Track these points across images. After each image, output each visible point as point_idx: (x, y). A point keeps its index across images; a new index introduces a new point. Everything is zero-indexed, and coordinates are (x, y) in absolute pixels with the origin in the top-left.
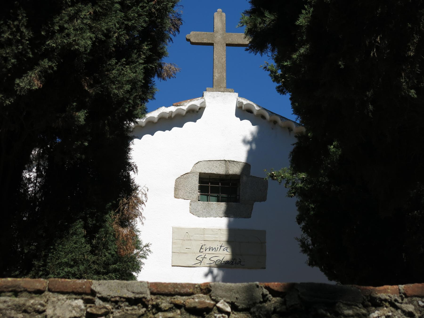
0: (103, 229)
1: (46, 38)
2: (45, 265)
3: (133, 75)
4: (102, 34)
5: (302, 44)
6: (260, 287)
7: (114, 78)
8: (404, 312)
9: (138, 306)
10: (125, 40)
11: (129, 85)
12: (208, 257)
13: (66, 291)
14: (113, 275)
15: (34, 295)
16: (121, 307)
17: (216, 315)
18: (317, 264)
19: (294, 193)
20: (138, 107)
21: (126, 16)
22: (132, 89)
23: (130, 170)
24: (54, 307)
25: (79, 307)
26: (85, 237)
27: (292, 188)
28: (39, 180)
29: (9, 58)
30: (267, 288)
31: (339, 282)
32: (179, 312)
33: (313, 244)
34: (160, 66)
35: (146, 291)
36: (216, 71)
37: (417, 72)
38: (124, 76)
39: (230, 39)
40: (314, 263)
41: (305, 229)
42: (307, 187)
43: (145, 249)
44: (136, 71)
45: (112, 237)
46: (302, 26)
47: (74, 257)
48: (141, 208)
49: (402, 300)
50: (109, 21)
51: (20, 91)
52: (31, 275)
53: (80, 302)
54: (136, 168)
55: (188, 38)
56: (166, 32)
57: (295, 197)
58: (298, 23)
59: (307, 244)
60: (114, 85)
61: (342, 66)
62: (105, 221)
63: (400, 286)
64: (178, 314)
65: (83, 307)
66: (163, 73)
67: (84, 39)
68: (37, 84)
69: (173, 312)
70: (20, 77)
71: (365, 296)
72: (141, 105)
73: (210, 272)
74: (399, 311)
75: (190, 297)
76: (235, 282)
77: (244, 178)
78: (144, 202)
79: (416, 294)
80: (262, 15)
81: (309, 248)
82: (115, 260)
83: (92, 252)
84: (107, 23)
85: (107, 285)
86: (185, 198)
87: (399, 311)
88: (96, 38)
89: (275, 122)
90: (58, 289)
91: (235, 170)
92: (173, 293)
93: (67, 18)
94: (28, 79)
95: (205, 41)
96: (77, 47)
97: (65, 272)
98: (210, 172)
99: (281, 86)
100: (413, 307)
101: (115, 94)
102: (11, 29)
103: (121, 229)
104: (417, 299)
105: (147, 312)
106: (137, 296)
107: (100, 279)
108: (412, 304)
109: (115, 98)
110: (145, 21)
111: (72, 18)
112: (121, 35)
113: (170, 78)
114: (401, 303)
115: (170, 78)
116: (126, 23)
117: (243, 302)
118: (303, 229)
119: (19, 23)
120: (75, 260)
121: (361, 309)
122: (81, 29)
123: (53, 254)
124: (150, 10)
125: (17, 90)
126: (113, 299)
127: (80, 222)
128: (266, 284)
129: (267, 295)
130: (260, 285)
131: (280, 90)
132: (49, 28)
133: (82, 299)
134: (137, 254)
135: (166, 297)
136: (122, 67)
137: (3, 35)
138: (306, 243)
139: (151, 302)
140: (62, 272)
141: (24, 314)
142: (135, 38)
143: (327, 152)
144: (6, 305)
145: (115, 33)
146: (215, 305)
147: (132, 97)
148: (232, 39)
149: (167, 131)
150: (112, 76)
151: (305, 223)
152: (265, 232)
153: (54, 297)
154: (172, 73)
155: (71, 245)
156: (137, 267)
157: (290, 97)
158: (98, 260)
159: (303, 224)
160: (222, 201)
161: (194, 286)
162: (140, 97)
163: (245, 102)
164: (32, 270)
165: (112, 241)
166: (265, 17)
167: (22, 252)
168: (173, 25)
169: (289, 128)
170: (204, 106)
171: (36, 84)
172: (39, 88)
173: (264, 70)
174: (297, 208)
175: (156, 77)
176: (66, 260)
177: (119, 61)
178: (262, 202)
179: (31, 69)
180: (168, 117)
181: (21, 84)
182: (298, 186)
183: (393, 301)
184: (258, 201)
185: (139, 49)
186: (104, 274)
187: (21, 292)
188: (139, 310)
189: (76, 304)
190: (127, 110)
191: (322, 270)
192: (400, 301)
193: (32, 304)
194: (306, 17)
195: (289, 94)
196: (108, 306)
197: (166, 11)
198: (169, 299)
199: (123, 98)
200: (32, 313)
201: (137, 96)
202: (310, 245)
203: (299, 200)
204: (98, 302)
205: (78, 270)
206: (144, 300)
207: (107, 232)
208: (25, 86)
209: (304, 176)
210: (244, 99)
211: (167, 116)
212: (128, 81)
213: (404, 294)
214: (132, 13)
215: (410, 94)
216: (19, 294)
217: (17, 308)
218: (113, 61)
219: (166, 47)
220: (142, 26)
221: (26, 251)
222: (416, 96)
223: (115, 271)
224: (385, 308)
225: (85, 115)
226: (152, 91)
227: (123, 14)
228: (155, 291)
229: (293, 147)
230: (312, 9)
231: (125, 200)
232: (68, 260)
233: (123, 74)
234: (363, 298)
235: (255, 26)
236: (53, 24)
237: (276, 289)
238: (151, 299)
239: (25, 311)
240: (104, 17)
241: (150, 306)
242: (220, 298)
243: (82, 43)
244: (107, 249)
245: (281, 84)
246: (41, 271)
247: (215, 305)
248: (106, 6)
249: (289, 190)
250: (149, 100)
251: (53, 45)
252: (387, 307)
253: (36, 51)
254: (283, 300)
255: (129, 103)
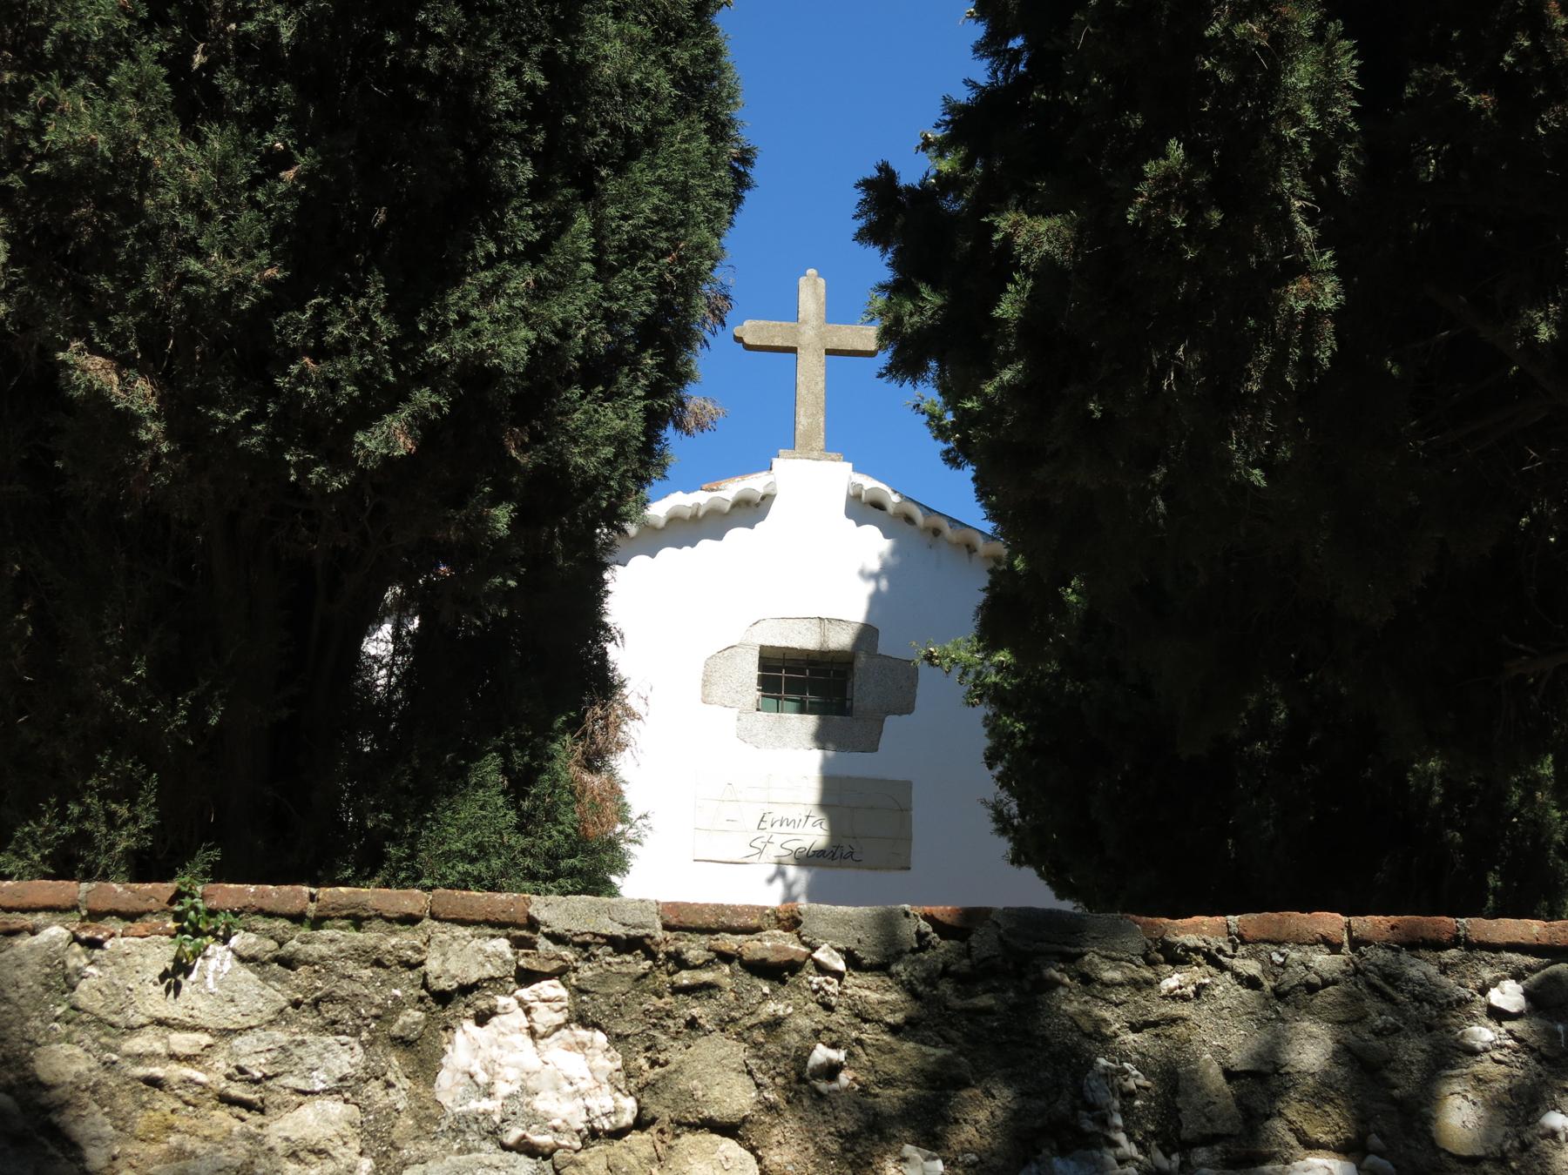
0: (546, 777)
1: (427, 338)
2: (412, 857)
3: (619, 424)
4: (552, 332)
5: (1007, 361)
6: (912, 916)
7: (575, 430)
8: (1237, 975)
9: (635, 956)
10: (602, 345)
11: (609, 446)
12: (778, 840)
13: (471, 917)
14: (566, 883)
15: (397, 927)
16: (595, 956)
17: (811, 978)
18: (1029, 862)
19: (980, 697)
20: (629, 497)
21: (606, 290)
22: (616, 456)
23: (607, 641)
24: (444, 954)
25: (500, 955)
26: (504, 793)
27: (975, 686)
28: (399, 660)
29: (342, 383)
30: (928, 918)
31: (1080, 904)
32: (727, 969)
33: (1022, 815)
34: (681, 404)
35: (654, 921)
36: (801, 411)
37: (1268, 429)
38: (598, 427)
39: (835, 339)
40: (1023, 858)
41: (1003, 780)
42: (1010, 684)
43: (639, 823)
44: (627, 415)
45: (565, 795)
46: (1006, 321)
47: (480, 839)
48: (631, 729)
49: (1235, 950)
50: (569, 302)
51: (366, 461)
52: (381, 879)
53: (502, 945)
54: (622, 637)
55: (737, 335)
56: (695, 327)
57: (982, 706)
58: (997, 313)
59: (1009, 815)
60: (577, 446)
61: (1098, 415)
62: (551, 758)
63: (1230, 917)
64: (726, 976)
65: (509, 956)
66: (688, 419)
67: (514, 344)
68: (404, 445)
69: (713, 971)
70: (365, 427)
71: (1151, 939)
72: (637, 492)
73: (781, 873)
74: (1228, 975)
75: (752, 937)
76: (856, 905)
77: (862, 660)
78: (643, 715)
79: (1265, 936)
80: (915, 294)
81: (1012, 825)
82: (572, 849)
83: (520, 829)
84: (565, 306)
85: (564, 906)
86: (726, 703)
87: (1228, 975)
88: (539, 339)
89: (936, 532)
90: (452, 913)
91: (841, 640)
92: (715, 926)
93: (476, 295)
94: (383, 433)
95: (778, 342)
96: (496, 361)
97: (459, 873)
98: (783, 644)
99: (953, 449)
100: (1259, 966)
101: (577, 467)
102: (349, 316)
103: (587, 777)
104: (1270, 947)
105: (654, 968)
106: (633, 932)
107: (549, 892)
108: (1257, 959)
109: (578, 476)
110: (649, 302)
111: (488, 294)
112: (594, 333)
113: (702, 431)
114: (1232, 957)
115: (702, 431)
116: (605, 304)
117: (874, 948)
118: (998, 779)
119: (369, 304)
120: (480, 847)
121: (1141, 970)
122: (509, 319)
123: (432, 831)
124: (661, 276)
125: (358, 457)
126: (576, 939)
127: (494, 758)
128: (927, 909)
129: (927, 934)
130: (912, 912)
131: (951, 459)
132: (437, 315)
133: (508, 937)
134: (623, 833)
135: (698, 935)
136: (596, 406)
137: (330, 329)
138: (1005, 811)
139: (663, 947)
140: (451, 874)
141: (375, 969)
142: (627, 340)
143: (1061, 606)
144: (334, 948)
145: (580, 327)
146: (809, 956)
147: (616, 475)
148: (839, 340)
149: (687, 549)
150: (573, 426)
151: (1004, 767)
152: (907, 785)
153: (442, 933)
154: (707, 419)
155: (473, 811)
156: (621, 866)
157: (973, 474)
158: (533, 846)
159: (999, 768)
160: (811, 712)
161: (752, 910)
162: (634, 476)
163: (869, 483)
164: (383, 869)
165: (567, 804)
166: (923, 299)
167: (360, 825)
168: (712, 312)
169: (968, 546)
170: (773, 493)
171: (402, 444)
172: (409, 454)
173: (915, 411)
174: (985, 731)
175: (670, 428)
176: (460, 845)
177: (588, 392)
178: (904, 717)
179: (392, 409)
180: (691, 517)
181: (367, 444)
182: (988, 680)
183: (1214, 952)
184: (895, 714)
185: (635, 366)
186: (546, 879)
187: (369, 918)
188: (637, 964)
189: (494, 949)
190: (604, 504)
191: (1041, 875)
192: (1230, 952)
193: (393, 947)
194: (1016, 301)
195: (971, 467)
196: (568, 954)
197: (697, 279)
198: (704, 939)
199: (595, 477)
200: (393, 968)
201: (627, 471)
202: (1014, 817)
203: (990, 713)
204: (544, 944)
205: (487, 868)
206: (648, 941)
207: (555, 784)
208: (377, 449)
209: (1002, 659)
210: (865, 477)
211: (688, 514)
212: (608, 438)
213: (1240, 936)
214: (620, 283)
215: (1252, 478)
216: (364, 924)
217: (360, 956)
218: (576, 392)
219: (696, 359)
220: (642, 313)
221: (370, 824)
222: (1264, 484)
223: (572, 873)
224: (1196, 968)
225: (510, 516)
226: (662, 462)
227: (600, 286)
228: (674, 922)
229: (983, 596)
230: (1029, 284)
231: (598, 709)
232: (465, 845)
233: (597, 422)
234: (1147, 944)
235: (898, 320)
236: (445, 308)
237: (948, 920)
238: (665, 939)
239: (378, 963)
240: (556, 293)
241: (661, 956)
242: (821, 941)
243: (509, 351)
244: (556, 822)
245: (952, 445)
246: (403, 869)
247: (809, 956)
248: (562, 266)
249: (967, 689)
250: (653, 481)
251: (443, 355)
252: (1199, 965)
253: (403, 368)
254: (964, 946)
255: (610, 488)
